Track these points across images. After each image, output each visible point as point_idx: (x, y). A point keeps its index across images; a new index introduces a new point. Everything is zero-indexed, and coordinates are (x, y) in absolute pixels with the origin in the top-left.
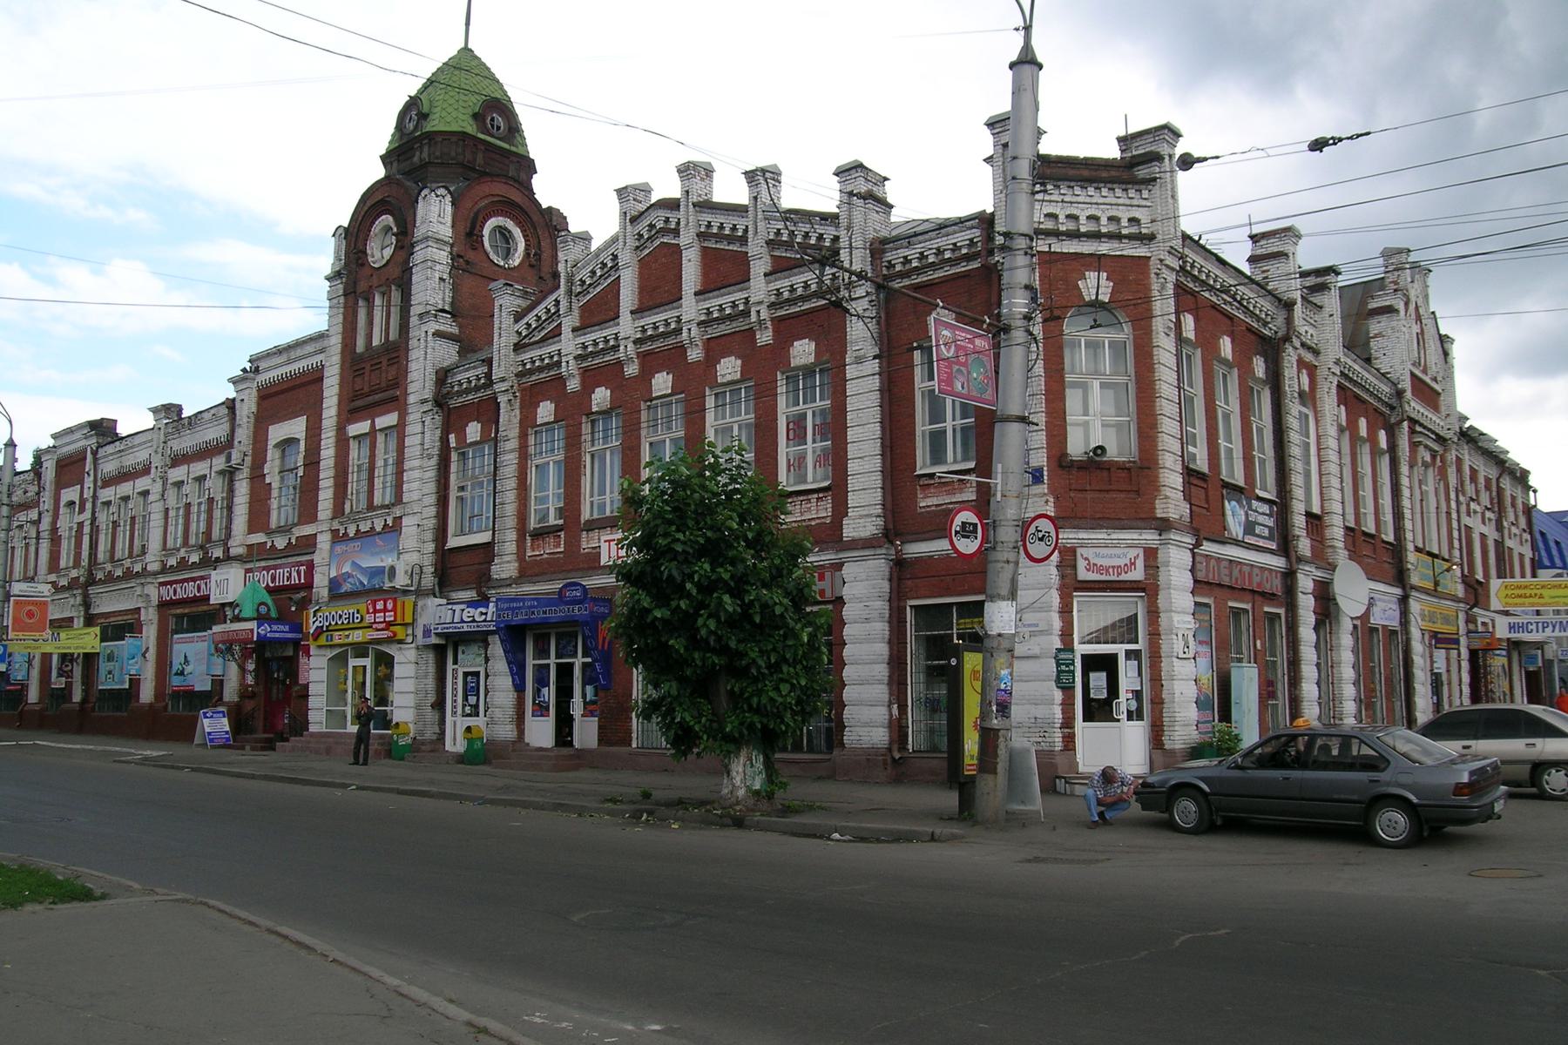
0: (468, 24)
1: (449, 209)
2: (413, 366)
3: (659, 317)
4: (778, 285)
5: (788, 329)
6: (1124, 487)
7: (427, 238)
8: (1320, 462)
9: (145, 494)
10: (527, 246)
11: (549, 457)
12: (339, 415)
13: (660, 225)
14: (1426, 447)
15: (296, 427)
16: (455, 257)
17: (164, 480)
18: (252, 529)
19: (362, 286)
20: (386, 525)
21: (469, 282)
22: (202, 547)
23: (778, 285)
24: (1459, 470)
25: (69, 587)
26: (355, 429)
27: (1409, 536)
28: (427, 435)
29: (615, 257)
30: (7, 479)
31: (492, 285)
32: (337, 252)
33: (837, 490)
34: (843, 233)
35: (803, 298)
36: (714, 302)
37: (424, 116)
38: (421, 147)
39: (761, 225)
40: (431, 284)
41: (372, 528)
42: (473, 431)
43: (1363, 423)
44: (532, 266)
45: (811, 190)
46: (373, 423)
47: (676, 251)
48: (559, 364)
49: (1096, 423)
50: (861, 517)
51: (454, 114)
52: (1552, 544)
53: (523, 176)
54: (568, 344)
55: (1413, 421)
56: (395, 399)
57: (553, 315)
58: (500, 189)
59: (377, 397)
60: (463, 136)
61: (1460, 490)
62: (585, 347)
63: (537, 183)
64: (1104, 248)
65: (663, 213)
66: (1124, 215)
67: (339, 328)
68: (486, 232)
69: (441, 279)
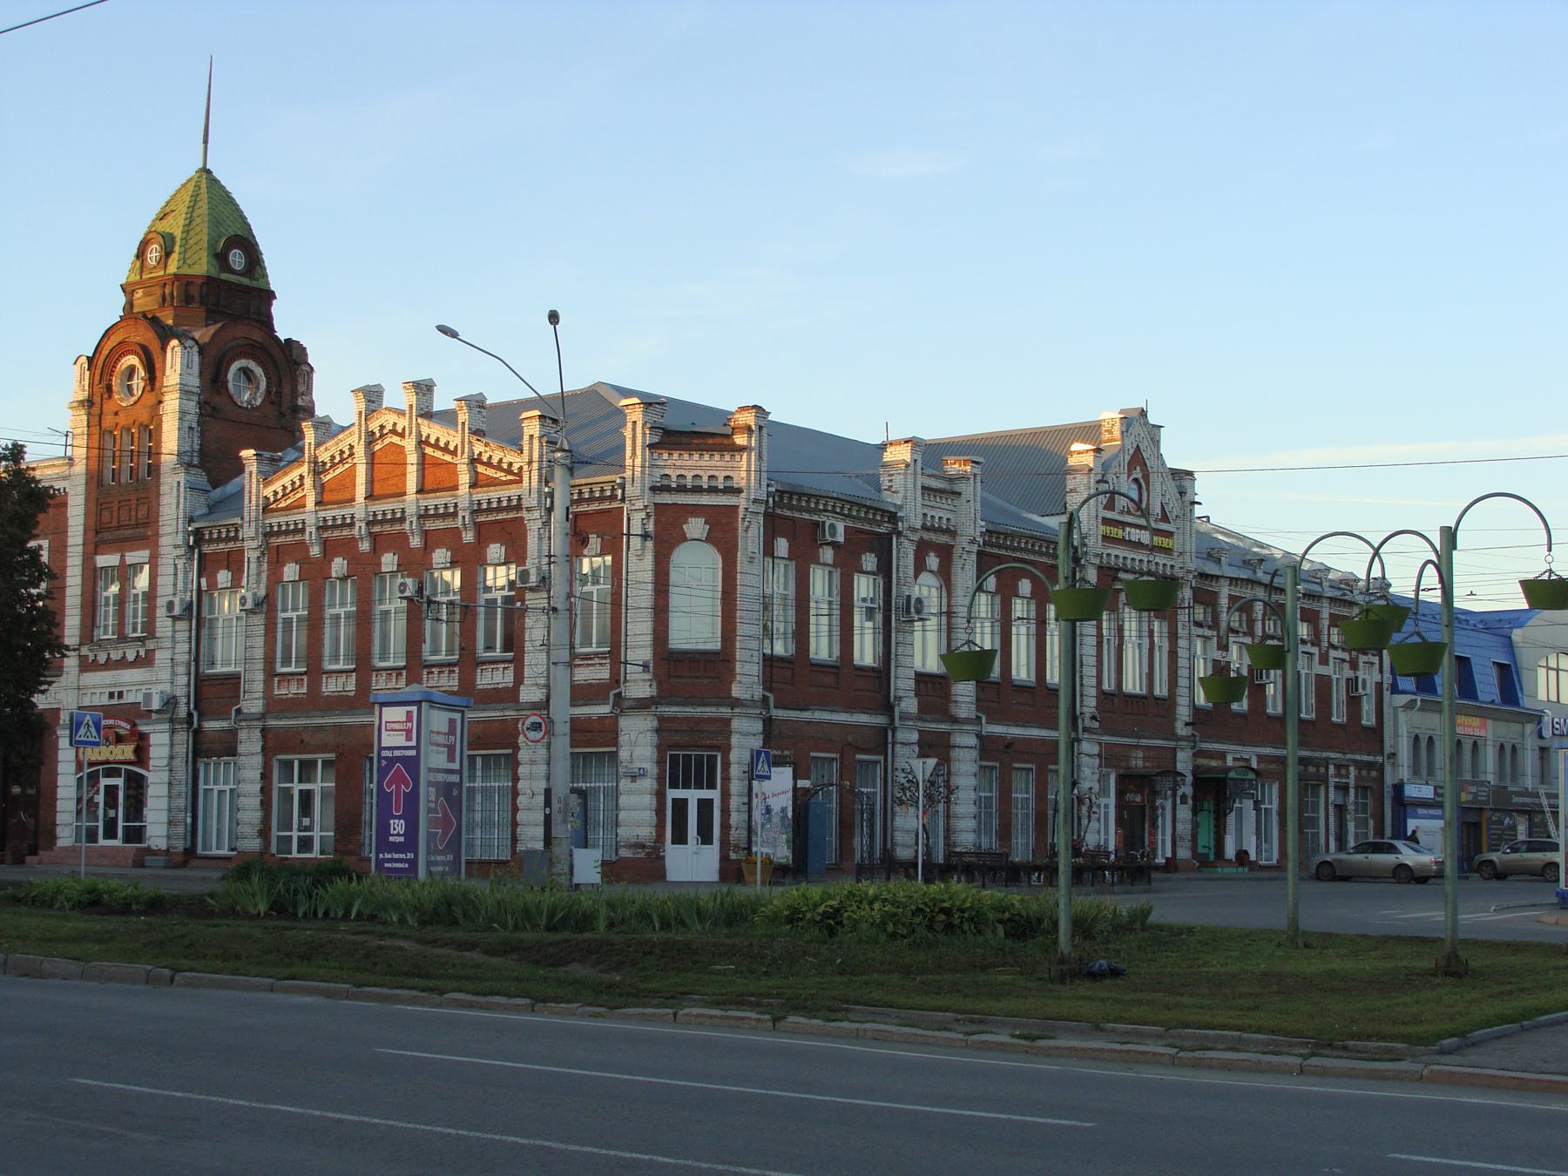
0: (206, 142)
1: (196, 359)
5: (485, 533)
26: (105, 560)
41: (124, 657)
46: (123, 556)
58: (242, 332)
62: (325, 520)
63: (276, 309)
64: (705, 500)
68: (230, 376)
69: (191, 428)
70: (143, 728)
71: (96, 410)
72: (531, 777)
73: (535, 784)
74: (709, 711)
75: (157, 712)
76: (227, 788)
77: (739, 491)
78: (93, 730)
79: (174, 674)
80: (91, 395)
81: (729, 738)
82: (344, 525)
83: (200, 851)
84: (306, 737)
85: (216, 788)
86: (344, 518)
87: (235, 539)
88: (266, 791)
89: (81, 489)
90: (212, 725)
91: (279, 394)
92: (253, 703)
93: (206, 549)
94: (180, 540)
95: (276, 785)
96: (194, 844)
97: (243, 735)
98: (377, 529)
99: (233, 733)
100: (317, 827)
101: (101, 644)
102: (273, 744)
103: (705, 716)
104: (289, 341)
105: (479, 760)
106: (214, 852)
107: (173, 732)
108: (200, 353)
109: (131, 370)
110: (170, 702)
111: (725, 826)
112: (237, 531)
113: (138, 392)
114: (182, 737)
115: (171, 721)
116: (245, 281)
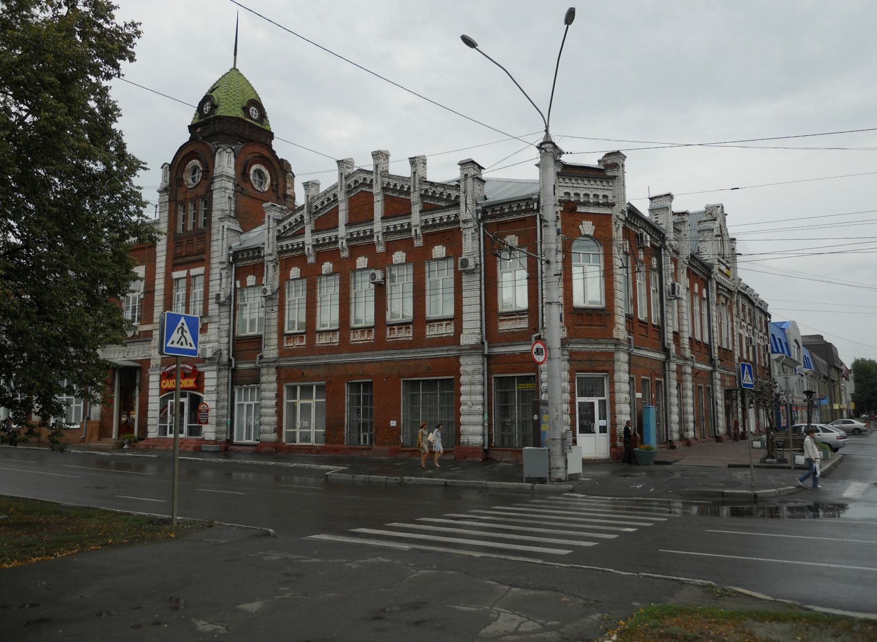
0: (235, 54)
1: (233, 160)
3: (360, 229)
6: (598, 323)
7: (222, 176)
8: (678, 306)
10: (272, 180)
11: (296, 297)
12: (166, 266)
13: (361, 181)
14: (724, 296)
16: (236, 186)
19: (180, 197)
23: (426, 217)
24: (737, 306)
26: (176, 275)
27: (716, 340)
28: (224, 280)
29: (335, 196)
31: (265, 205)
32: (164, 176)
33: (457, 319)
34: (462, 195)
35: (440, 225)
37: (214, 107)
38: (214, 124)
42: (251, 280)
43: (696, 286)
44: (274, 191)
45: (442, 171)
47: (371, 195)
48: (303, 248)
49: (588, 290)
50: (470, 334)
51: (233, 107)
52: (777, 341)
54: (308, 239)
55: (718, 283)
56: (203, 260)
61: (738, 316)
63: (275, 145)
64: (592, 210)
65: (363, 175)
66: (601, 193)
67: (166, 219)
68: (251, 172)
69: (229, 198)
70: (201, 369)
72: (470, 393)
74: (601, 348)
75: (209, 359)
76: (253, 403)
77: (613, 205)
78: (188, 335)
80: (171, 184)
82: (330, 243)
83: (235, 441)
85: (246, 403)
87: (259, 257)
88: (279, 405)
91: (277, 185)
92: (271, 351)
93: (240, 264)
94: (224, 259)
95: (285, 401)
96: (232, 437)
97: (264, 371)
99: (258, 370)
100: (313, 427)
102: (285, 376)
104: (282, 160)
106: (245, 441)
107: (219, 370)
108: (235, 157)
109: (195, 168)
113: (198, 180)
115: (218, 364)
116: (259, 125)
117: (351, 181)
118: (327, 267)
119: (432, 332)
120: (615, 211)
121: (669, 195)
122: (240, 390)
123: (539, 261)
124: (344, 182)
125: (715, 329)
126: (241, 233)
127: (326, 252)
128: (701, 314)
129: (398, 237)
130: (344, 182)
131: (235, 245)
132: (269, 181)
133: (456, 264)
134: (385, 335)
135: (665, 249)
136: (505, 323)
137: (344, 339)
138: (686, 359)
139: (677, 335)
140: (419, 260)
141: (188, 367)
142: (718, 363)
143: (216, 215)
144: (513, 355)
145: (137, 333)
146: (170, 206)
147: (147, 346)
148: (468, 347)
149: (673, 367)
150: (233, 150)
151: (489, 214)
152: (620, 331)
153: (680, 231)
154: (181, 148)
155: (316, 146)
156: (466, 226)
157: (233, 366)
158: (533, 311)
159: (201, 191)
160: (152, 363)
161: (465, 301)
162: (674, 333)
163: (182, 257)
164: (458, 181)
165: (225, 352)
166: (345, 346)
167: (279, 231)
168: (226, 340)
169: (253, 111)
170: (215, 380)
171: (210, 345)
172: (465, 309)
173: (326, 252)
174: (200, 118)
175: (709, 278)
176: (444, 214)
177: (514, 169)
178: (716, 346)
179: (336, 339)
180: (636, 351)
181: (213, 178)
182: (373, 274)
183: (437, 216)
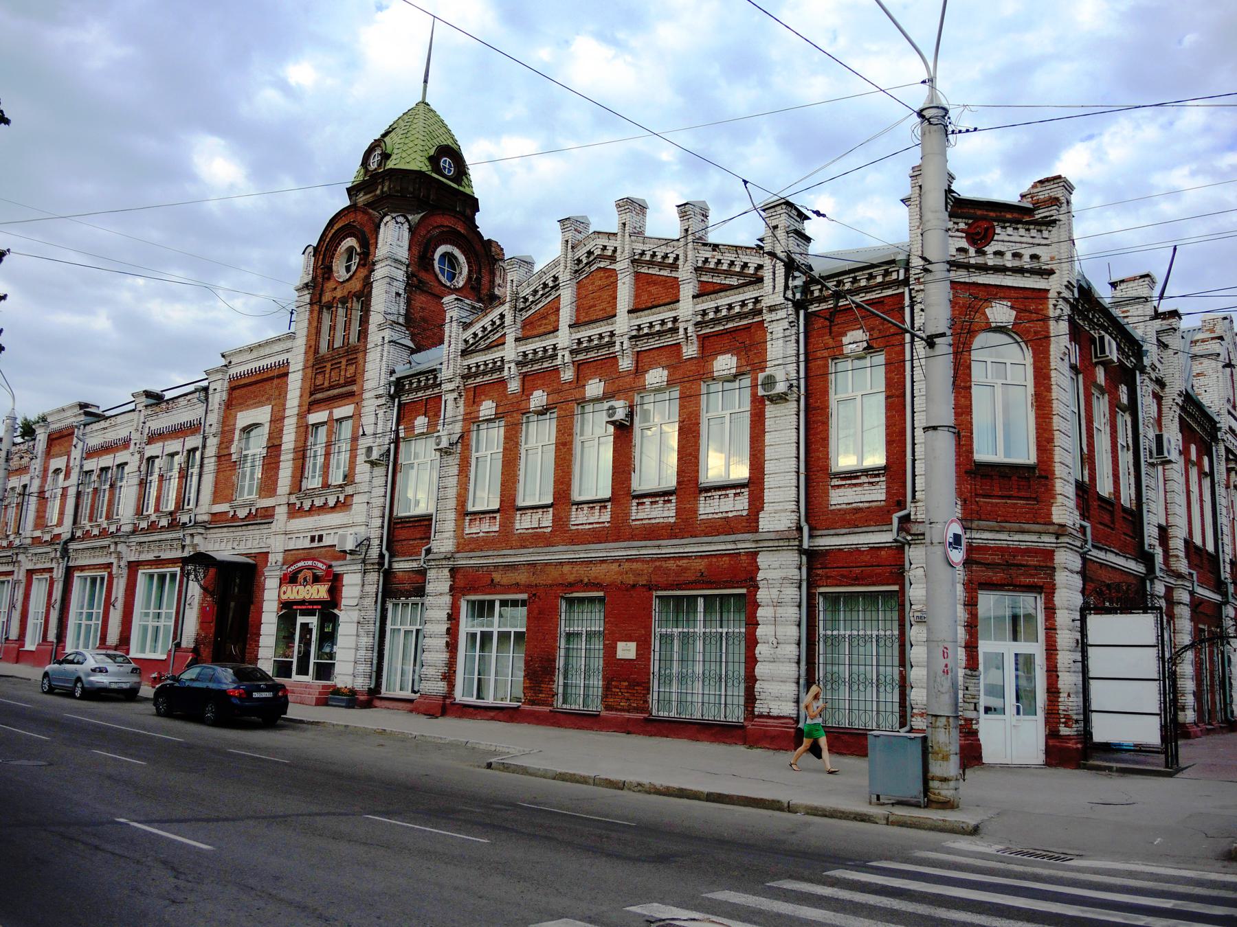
0: (426, 81)
2: (368, 366)
4: (705, 306)
5: (710, 345)
6: (1023, 494)
9: (122, 466)
10: (470, 271)
15: (262, 414)
17: (141, 453)
18: (215, 501)
20: (338, 501)
21: (420, 300)
22: (171, 513)
25: (51, 543)
26: (314, 418)
29: (555, 279)
30: (5, 446)
33: (755, 485)
35: (728, 319)
36: (645, 319)
37: (386, 156)
39: (690, 254)
40: (386, 297)
42: (421, 422)
43: (1193, 448)
44: (473, 288)
46: (331, 413)
49: (1003, 437)
53: (468, 212)
54: (510, 351)
56: (352, 394)
57: (499, 325)
58: (448, 221)
59: (336, 392)
60: (419, 173)
63: (479, 219)
65: (602, 241)
67: (305, 332)
68: (437, 256)
69: (398, 294)
70: (337, 570)
71: (318, 289)
73: (781, 630)
75: (352, 552)
77: (1051, 272)
79: (369, 516)
80: (314, 278)
81: (1052, 576)
84: (497, 577)
86: (545, 350)
88: (452, 632)
89: (301, 358)
90: (401, 565)
91: (478, 280)
92: (443, 542)
97: (431, 574)
98: (581, 357)
99: (422, 573)
101: (310, 494)
102: (462, 582)
103: (1023, 546)
105: (701, 601)
108: (410, 229)
109: (350, 250)
110: (365, 543)
111: (1053, 691)
112: (435, 378)
114: (373, 577)
115: (364, 561)
117: (581, 253)
118: (538, 398)
119: (708, 508)
120: (1054, 285)
121: (1147, 276)
122: (396, 605)
123: (908, 336)
124: (570, 255)
125: (1225, 528)
126: (413, 352)
127: (536, 374)
128: (1201, 501)
129: (654, 343)
130: (570, 255)
131: (402, 370)
132: (465, 270)
133: (754, 386)
134: (628, 514)
135: (1143, 371)
136: (841, 491)
137: (560, 522)
138: (1179, 576)
139: (1163, 531)
140: (690, 381)
141: (320, 565)
142: (1231, 589)
143: (375, 319)
144: (856, 551)
145: (253, 511)
146: (311, 312)
147: (264, 530)
148: (772, 536)
149: (1160, 588)
150: (408, 220)
151: (816, 294)
152: (1064, 511)
153: (1166, 346)
154: (331, 221)
155: (523, 196)
156: (773, 316)
157: (386, 566)
158: (895, 470)
159: (356, 285)
160: (271, 558)
161: (769, 453)
162: (1160, 527)
163: (323, 390)
164: (761, 240)
165: (376, 542)
166: (562, 532)
167: (466, 341)
168: (378, 522)
169: (445, 162)
170: (358, 588)
171: (352, 530)
172: (769, 467)
173: (536, 372)
174: (365, 174)
175: (1215, 439)
176: (734, 298)
177: (862, 218)
178: (1228, 560)
179: (547, 520)
180: (1095, 552)
181: (374, 264)
182: (612, 408)
183: (723, 301)
